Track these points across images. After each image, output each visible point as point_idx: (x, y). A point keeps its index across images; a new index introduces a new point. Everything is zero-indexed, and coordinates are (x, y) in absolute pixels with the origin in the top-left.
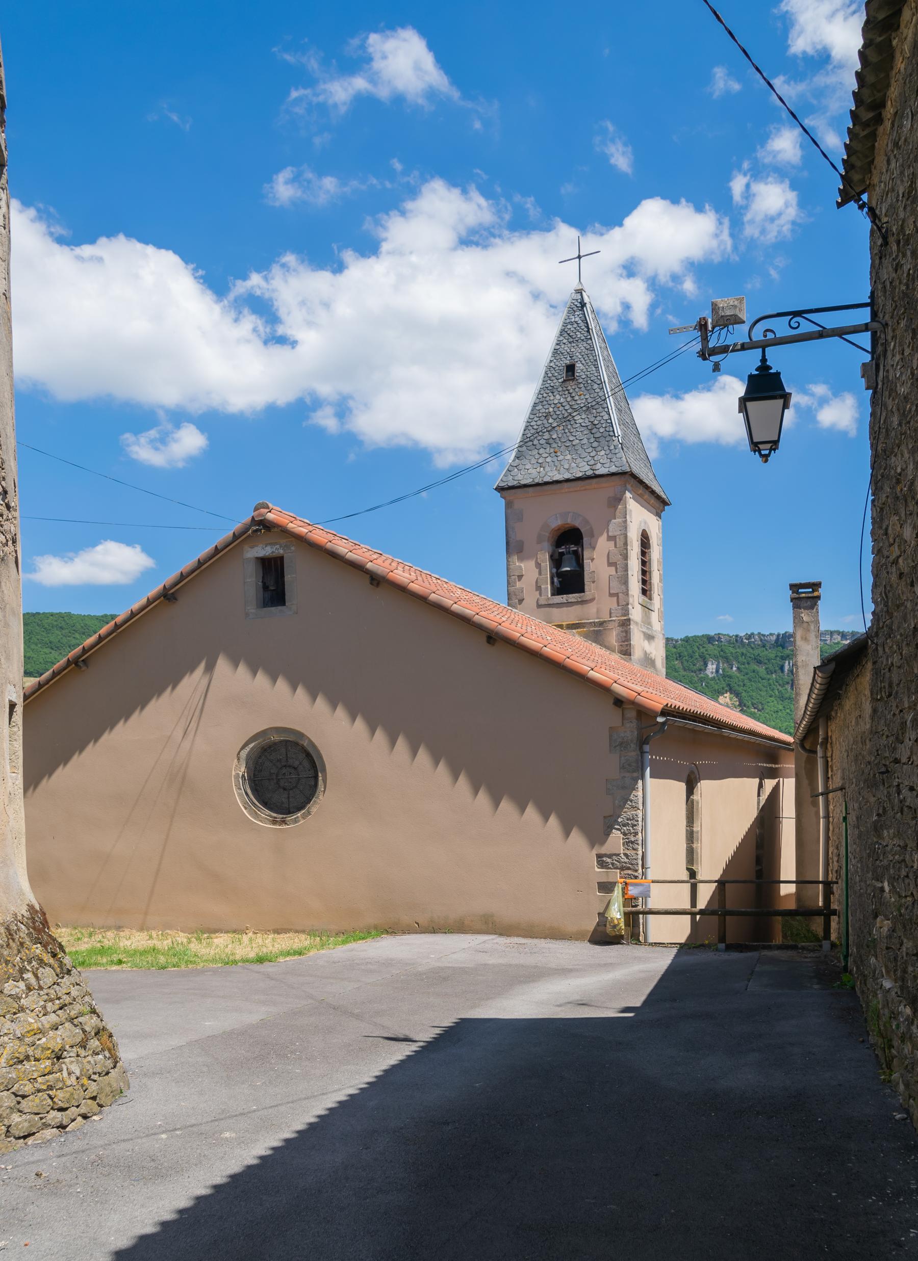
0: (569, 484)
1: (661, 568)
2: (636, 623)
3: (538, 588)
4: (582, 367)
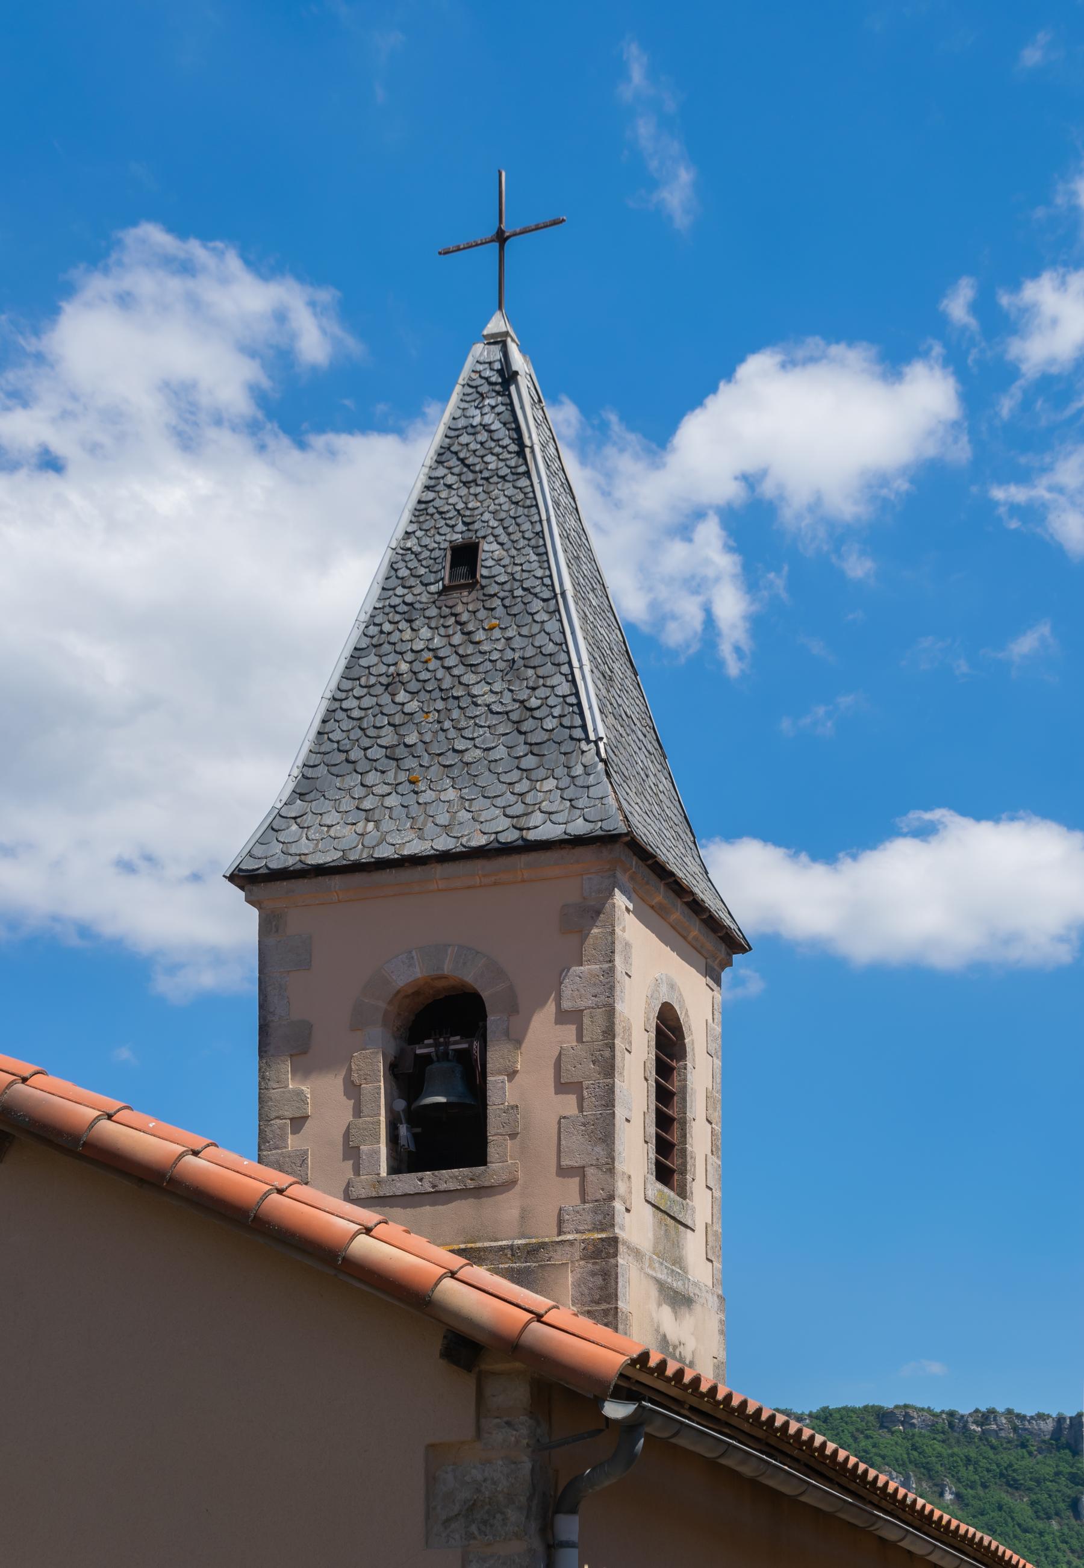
0: (450, 868)
1: (716, 1116)
2: (637, 1254)
3: (351, 1152)
4: (499, 553)
